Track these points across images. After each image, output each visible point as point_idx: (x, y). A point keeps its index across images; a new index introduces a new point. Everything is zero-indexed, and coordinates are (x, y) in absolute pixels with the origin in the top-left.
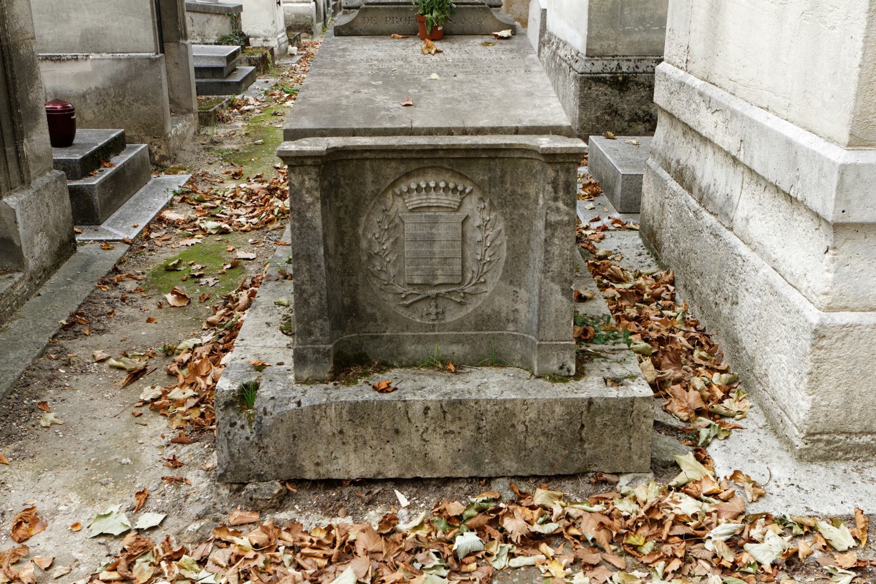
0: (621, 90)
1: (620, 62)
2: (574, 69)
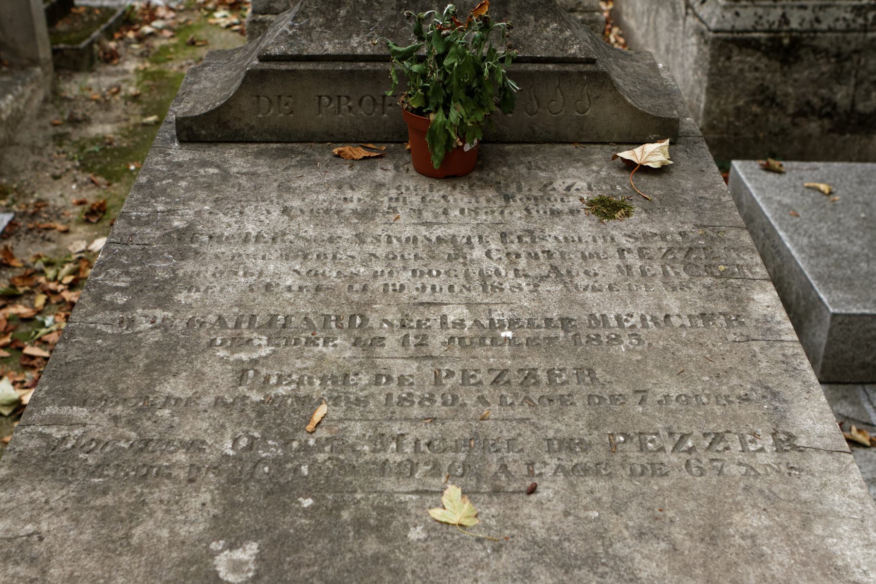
0: (784, 62)
1: (788, 10)
2: (696, 15)
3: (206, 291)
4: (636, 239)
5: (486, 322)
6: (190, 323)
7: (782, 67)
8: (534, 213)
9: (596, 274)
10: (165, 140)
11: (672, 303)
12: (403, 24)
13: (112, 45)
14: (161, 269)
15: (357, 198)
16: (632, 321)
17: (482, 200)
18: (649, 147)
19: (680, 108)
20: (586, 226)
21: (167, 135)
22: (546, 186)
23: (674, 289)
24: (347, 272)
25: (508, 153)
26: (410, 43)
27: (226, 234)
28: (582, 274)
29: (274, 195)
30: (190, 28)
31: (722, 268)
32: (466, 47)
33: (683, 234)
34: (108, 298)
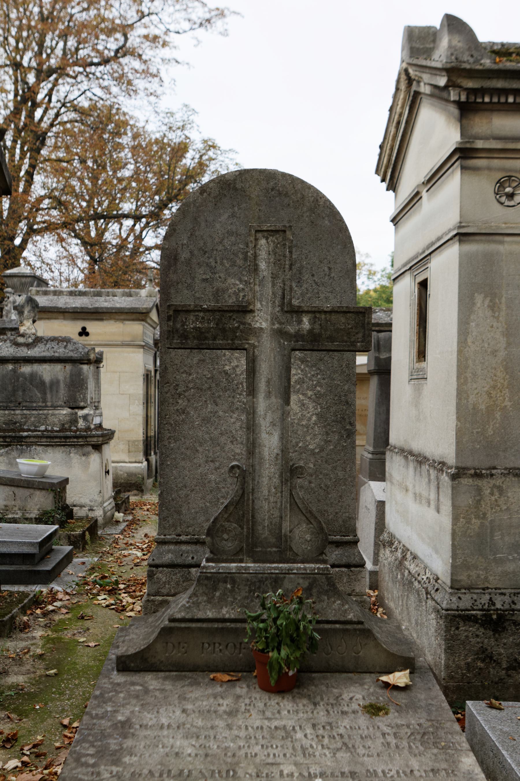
0: (495, 631)
1: (493, 596)
2: (433, 599)
3: (141, 756)
4: (392, 728)
5: (306, 774)
6: (133, 774)
7: (494, 635)
8: (331, 712)
9: (369, 747)
10: (108, 670)
11: (414, 763)
12: (252, 601)
13: (25, 618)
14: (113, 744)
15: (226, 704)
16: (392, 773)
17: (300, 705)
18: (397, 674)
19: (416, 652)
20: (363, 720)
21: (109, 667)
22: (337, 697)
23: (415, 755)
24: (223, 746)
25: (314, 678)
26: (256, 612)
27: (150, 724)
28: (361, 747)
29: (176, 702)
30: (80, 606)
31: (443, 744)
32: (290, 613)
33: (420, 725)
34: (83, 760)
